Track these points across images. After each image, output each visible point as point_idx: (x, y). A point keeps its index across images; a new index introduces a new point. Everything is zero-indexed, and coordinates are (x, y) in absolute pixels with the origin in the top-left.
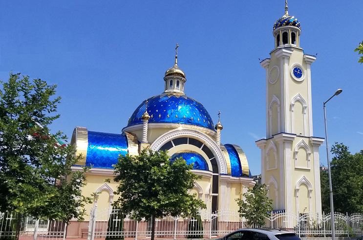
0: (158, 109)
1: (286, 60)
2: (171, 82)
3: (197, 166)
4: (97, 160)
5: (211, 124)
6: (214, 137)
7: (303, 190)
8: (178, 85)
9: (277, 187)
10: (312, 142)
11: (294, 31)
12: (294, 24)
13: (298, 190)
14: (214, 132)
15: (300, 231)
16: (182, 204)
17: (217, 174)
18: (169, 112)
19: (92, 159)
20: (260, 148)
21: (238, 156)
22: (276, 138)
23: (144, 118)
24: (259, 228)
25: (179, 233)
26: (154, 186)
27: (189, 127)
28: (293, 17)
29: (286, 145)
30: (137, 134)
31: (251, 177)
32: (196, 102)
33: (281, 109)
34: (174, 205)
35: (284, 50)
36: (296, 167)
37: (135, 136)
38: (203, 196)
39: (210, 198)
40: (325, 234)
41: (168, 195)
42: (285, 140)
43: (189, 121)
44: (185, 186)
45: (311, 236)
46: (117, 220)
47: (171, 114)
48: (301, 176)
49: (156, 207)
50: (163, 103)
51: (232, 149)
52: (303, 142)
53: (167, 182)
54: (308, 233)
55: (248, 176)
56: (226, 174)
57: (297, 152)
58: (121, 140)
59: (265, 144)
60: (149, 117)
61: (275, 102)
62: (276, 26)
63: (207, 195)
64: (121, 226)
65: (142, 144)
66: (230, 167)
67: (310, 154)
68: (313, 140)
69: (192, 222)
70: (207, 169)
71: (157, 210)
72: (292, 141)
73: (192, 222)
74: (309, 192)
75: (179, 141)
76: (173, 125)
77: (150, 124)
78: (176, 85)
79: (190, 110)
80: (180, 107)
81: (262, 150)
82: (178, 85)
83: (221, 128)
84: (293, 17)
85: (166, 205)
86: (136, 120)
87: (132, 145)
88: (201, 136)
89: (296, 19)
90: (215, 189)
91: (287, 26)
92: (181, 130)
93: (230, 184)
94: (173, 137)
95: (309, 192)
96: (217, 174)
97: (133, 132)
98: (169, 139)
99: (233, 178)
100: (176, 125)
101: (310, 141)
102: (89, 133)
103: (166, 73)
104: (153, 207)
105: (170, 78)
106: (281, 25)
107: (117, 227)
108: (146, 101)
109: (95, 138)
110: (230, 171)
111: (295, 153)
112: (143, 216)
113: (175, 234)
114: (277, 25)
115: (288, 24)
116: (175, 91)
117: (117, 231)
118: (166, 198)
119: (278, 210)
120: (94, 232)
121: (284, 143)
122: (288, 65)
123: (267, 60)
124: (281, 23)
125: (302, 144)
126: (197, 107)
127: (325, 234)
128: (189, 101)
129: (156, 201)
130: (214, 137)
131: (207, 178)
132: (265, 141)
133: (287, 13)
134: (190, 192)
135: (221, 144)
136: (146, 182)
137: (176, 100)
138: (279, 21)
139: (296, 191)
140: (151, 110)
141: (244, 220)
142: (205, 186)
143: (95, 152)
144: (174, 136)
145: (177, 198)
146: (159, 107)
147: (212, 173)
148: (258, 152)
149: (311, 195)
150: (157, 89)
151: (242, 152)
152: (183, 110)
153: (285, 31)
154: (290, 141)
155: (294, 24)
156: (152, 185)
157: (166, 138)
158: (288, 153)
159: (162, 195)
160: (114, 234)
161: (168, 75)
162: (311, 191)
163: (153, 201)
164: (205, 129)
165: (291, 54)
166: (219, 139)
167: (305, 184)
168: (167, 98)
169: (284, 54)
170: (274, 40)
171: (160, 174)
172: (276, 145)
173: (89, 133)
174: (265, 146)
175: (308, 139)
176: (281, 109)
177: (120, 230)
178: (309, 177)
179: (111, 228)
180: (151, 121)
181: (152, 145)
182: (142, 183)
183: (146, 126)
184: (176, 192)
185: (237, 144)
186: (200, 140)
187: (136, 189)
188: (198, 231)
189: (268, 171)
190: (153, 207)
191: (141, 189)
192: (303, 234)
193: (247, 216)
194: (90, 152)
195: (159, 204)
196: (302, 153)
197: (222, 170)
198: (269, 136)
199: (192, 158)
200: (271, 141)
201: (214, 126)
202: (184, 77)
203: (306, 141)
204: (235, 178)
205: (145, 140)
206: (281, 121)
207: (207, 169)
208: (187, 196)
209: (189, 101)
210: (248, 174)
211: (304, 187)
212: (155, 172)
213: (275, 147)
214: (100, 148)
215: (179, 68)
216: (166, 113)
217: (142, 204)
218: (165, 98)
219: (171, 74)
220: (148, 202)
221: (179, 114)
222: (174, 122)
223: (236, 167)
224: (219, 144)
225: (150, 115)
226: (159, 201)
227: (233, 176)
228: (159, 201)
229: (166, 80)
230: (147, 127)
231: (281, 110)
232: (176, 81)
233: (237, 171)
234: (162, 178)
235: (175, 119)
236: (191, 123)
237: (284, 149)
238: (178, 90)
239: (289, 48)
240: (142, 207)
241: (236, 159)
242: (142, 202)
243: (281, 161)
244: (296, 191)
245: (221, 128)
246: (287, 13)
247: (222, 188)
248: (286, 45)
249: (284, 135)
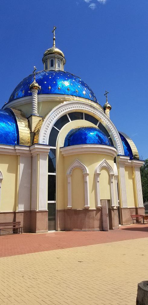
23: (33, 87)
83: (109, 108)
94: (69, 110)
103: (44, 54)
169: (37, 150)
215: (57, 47)
230: (36, 100)
238: (59, 67)
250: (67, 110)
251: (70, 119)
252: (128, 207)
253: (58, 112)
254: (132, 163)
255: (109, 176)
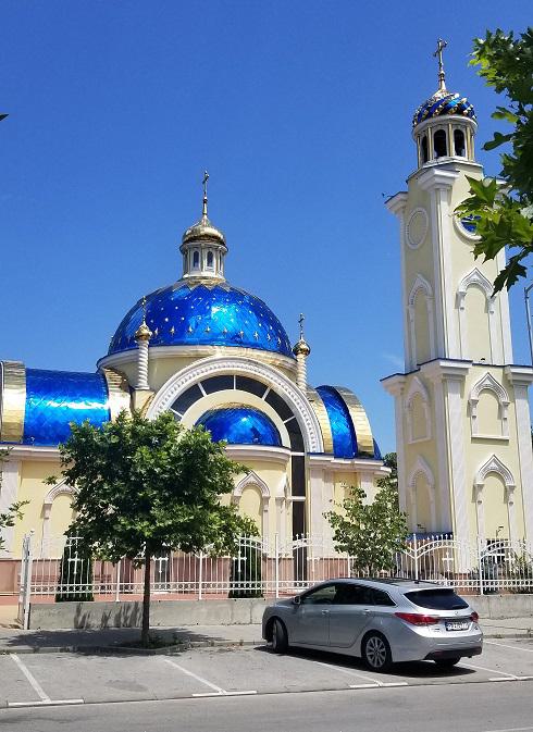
0: (170, 318)
1: (443, 194)
2: (196, 255)
3: (256, 437)
4: (46, 430)
5: (283, 344)
6: (292, 373)
7: (494, 486)
8: (210, 261)
9: (431, 480)
10: (511, 377)
11: (459, 128)
12: (460, 110)
13: (481, 487)
14: (291, 361)
15: (481, 580)
16: (202, 528)
17: (302, 454)
18: (192, 322)
19: (36, 428)
20: (392, 393)
21: (347, 411)
22: (426, 370)
23: (139, 337)
24: (372, 577)
25: (208, 586)
26: (143, 489)
27: (236, 352)
28: (457, 95)
29: (449, 386)
30: (129, 371)
31: (379, 458)
32: (251, 298)
33: (434, 304)
34: (185, 528)
35: (437, 172)
36: (474, 435)
37: (123, 375)
38: (272, 502)
39: (287, 507)
40: (482, 587)
41: (172, 507)
42: (445, 375)
43: (235, 340)
44: (213, 487)
45: (512, 591)
46: (76, 560)
47: (197, 325)
48: (487, 454)
49: (146, 534)
50: (177, 302)
51: (333, 397)
52: (490, 377)
53: (170, 478)
54: (501, 583)
55: (375, 455)
56: (321, 454)
57: (475, 402)
58: (93, 385)
59: (402, 386)
60: (151, 333)
61: (421, 290)
62: (420, 118)
63: (279, 501)
64: (85, 572)
65: (137, 393)
66: (329, 435)
67: (506, 405)
68: (514, 374)
69: (73, 563)
70: (277, 442)
71: (149, 540)
72: (464, 377)
73: (73, 563)
74: (508, 490)
75: (216, 383)
76: (201, 349)
77: (154, 349)
78: (205, 262)
79: (238, 316)
80: (215, 310)
81: (396, 398)
82: (210, 261)
83: (307, 352)
84: (457, 95)
85: (168, 530)
86: (124, 341)
87: (117, 394)
88: (263, 371)
89: (465, 100)
90: (299, 486)
91: (443, 117)
92: (221, 359)
93: (330, 475)
94: (201, 375)
95: (508, 490)
96: (302, 454)
97: (118, 368)
98: (193, 379)
99: (336, 461)
100: (208, 349)
101: (505, 376)
102: (29, 372)
103: (185, 236)
104: (142, 532)
105: (194, 247)
106: (429, 116)
107: (78, 575)
108: (142, 300)
109: (41, 383)
110: (330, 446)
111: (472, 404)
112: (122, 551)
113: (200, 589)
114: (420, 115)
115: (446, 110)
116: (204, 274)
117: (242, 580)
118: (169, 515)
119: (439, 533)
120: (29, 586)
121: (444, 381)
122: (449, 204)
123: (401, 196)
124: (430, 110)
125: (488, 382)
126: (252, 308)
127: (482, 587)
128: (234, 296)
129: (147, 520)
130: (292, 373)
131: (275, 463)
132: (402, 379)
133: (444, 87)
134: (224, 500)
135: (308, 387)
136: (126, 479)
137: (207, 295)
138: (425, 107)
139: (477, 489)
140: (154, 319)
141: (350, 558)
142: (279, 481)
143: (42, 414)
144: (205, 374)
145: (191, 514)
146: (170, 312)
147: (288, 452)
148: (388, 403)
149: (512, 497)
150: (164, 274)
151: (356, 402)
152: (222, 315)
153: (439, 128)
154: (458, 376)
155: (460, 110)
156: (138, 486)
157: (187, 378)
158: (455, 404)
159: (159, 506)
160: (253, 586)
161: (187, 242)
162: (512, 488)
163: (142, 520)
164: (271, 355)
165: (453, 178)
166: (302, 377)
167: (499, 472)
168: (187, 291)
169: (437, 180)
170: (414, 149)
171: (152, 461)
172: (426, 386)
173: (29, 372)
174: (402, 389)
175: (501, 370)
176: (434, 304)
177: (85, 582)
178: (505, 456)
179: (65, 577)
180: (154, 342)
181: (158, 394)
182: (118, 483)
183: (144, 353)
184: (190, 501)
185: (342, 386)
186: (260, 380)
187: (105, 495)
188: (251, 582)
189: (413, 444)
190: (142, 532)
191: (117, 495)
192: (490, 586)
193: (350, 550)
194: (31, 412)
195: (152, 528)
196: (488, 403)
197: (311, 445)
198: (412, 367)
199: (244, 419)
200: (415, 377)
201: (292, 347)
202: (222, 243)
203: (497, 375)
204: (342, 461)
205: (144, 383)
206: (435, 332)
207: (277, 442)
208: (217, 508)
209: (234, 296)
210: (372, 451)
211: (494, 480)
212: (142, 459)
213: (423, 392)
214: (53, 404)
215: (212, 225)
216: (185, 325)
217: (119, 528)
218: (182, 293)
219: (195, 238)
220: (131, 523)
221: (214, 325)
222: (203, 343)
223: (343, 437)
224: (303, 386)
225: (152, 330)
226: (152, 520)
227: (337, 456)
228: (152, 520)
229: (184, 251)
230: (146, 357)
231: (434, 308)
232: (205, 253)
233: (346, 446)
234: (157, 470)
235: (205, 336)
236: (241, 343)
237: (445, 395)
238: (211, 273)
239: (450, 166)
240: (120, 535)
241: (344, 419)
242: (119, 523)
243: (439, 423)
244: (477, 489)
245: (307, 352)
246: (444, 87)
247: (314, 484)
248: (443, 158)
249: (443, 364)
250: (198, 377)
251: (203, 392)
252: (14, 559)
253: (180, 383)
254: (353, 464)
255: (262, 499)
